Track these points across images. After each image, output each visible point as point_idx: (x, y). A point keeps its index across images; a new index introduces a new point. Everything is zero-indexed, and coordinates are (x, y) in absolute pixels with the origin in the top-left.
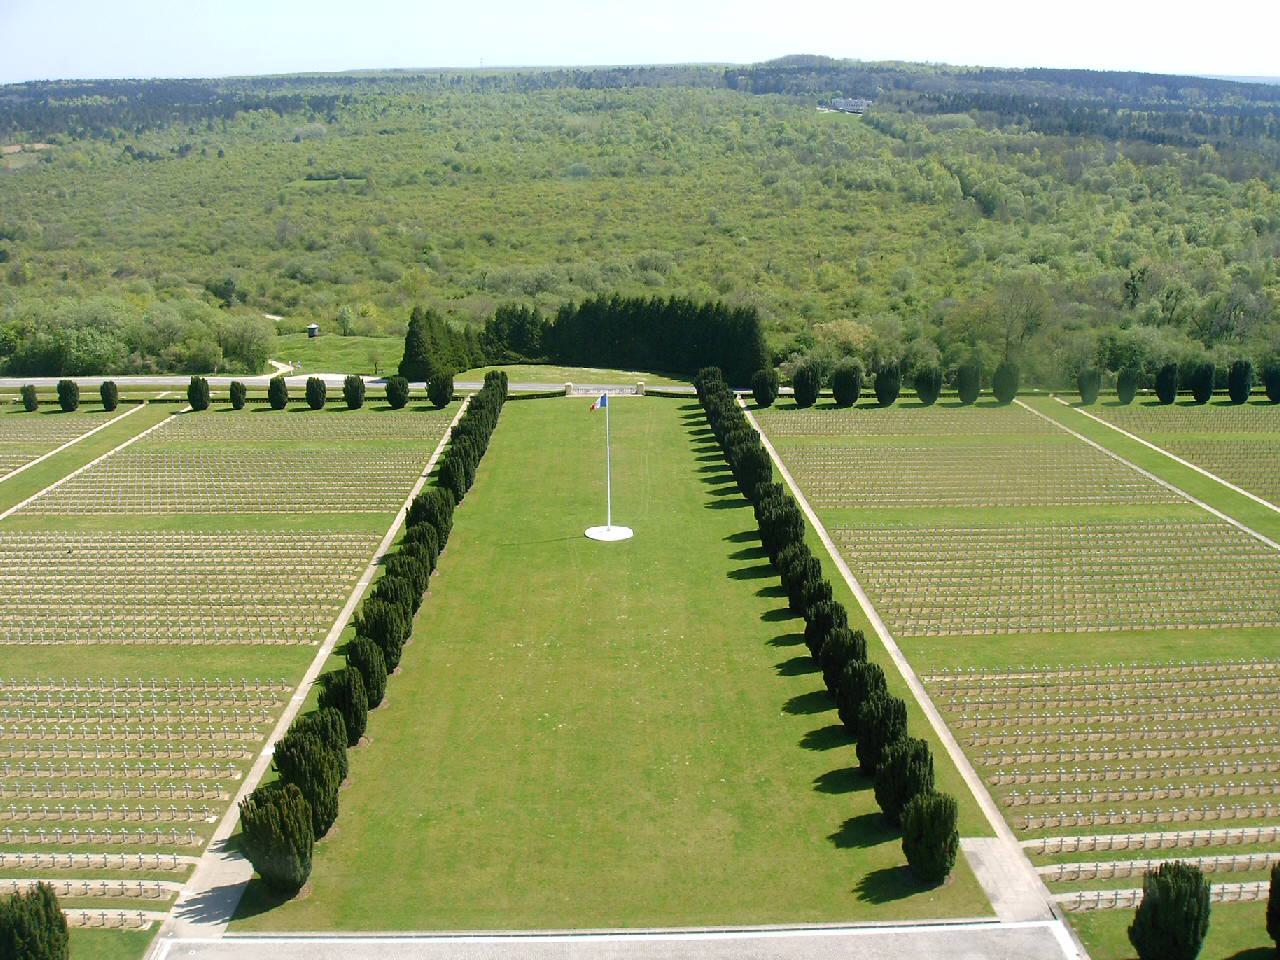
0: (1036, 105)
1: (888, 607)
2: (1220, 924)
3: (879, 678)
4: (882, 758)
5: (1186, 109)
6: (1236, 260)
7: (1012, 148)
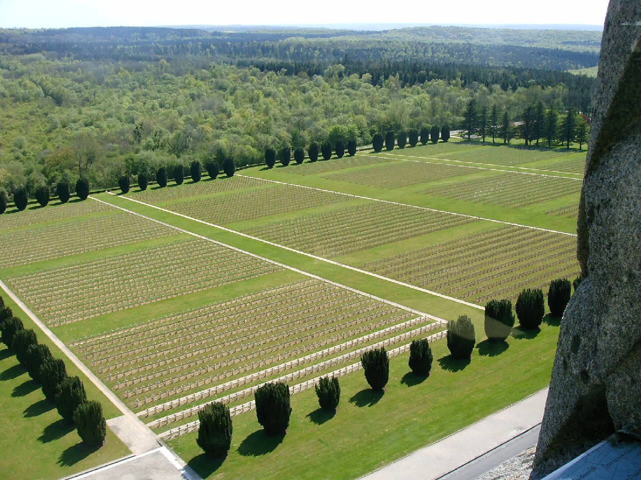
0: (76, 46)
1: (44, 314)
2: (237, 426)
3: (46, 351)
4: (56, 391)
5: (151, 43)
6: (184, 114)
7: (67, 69)
